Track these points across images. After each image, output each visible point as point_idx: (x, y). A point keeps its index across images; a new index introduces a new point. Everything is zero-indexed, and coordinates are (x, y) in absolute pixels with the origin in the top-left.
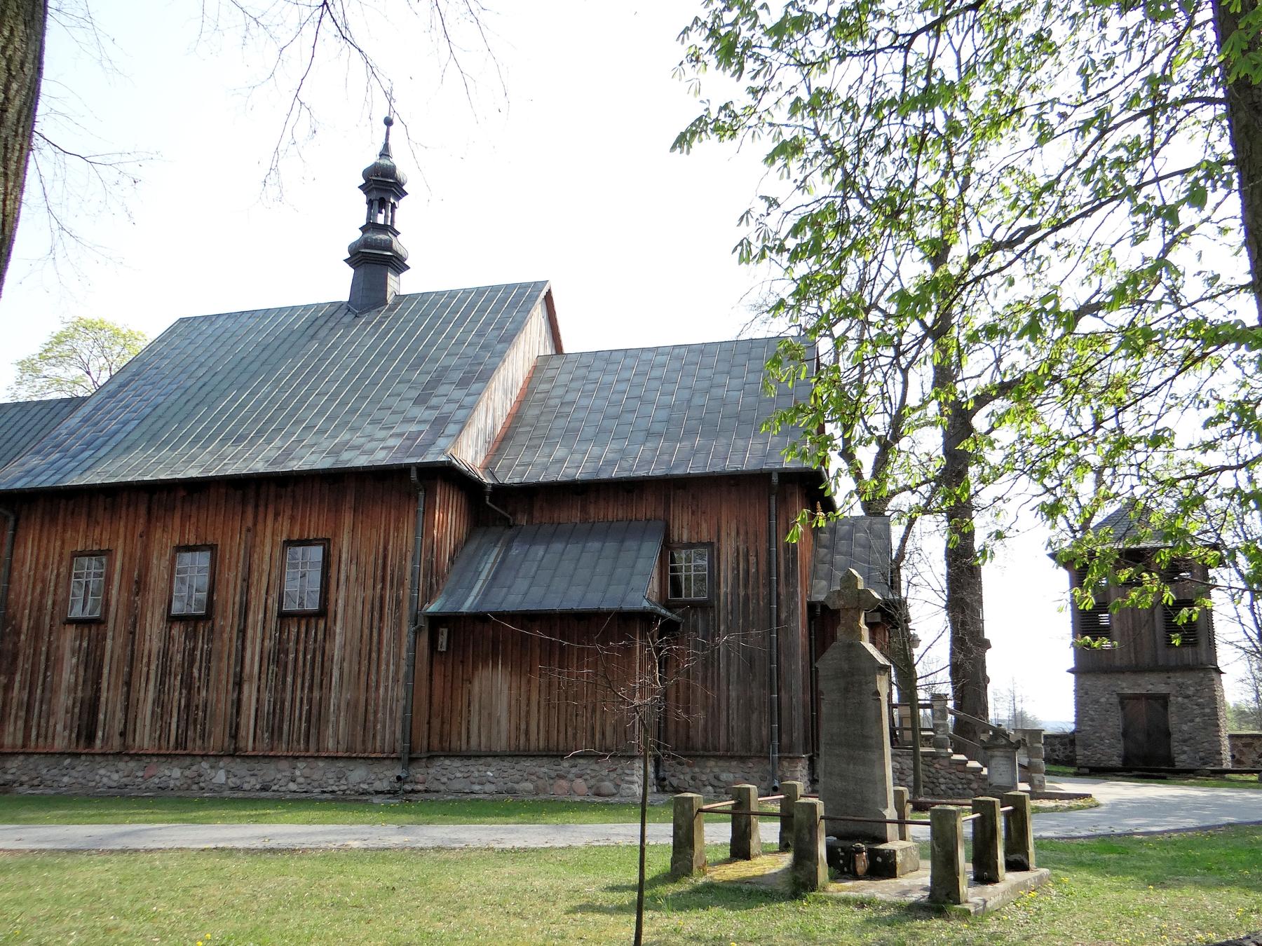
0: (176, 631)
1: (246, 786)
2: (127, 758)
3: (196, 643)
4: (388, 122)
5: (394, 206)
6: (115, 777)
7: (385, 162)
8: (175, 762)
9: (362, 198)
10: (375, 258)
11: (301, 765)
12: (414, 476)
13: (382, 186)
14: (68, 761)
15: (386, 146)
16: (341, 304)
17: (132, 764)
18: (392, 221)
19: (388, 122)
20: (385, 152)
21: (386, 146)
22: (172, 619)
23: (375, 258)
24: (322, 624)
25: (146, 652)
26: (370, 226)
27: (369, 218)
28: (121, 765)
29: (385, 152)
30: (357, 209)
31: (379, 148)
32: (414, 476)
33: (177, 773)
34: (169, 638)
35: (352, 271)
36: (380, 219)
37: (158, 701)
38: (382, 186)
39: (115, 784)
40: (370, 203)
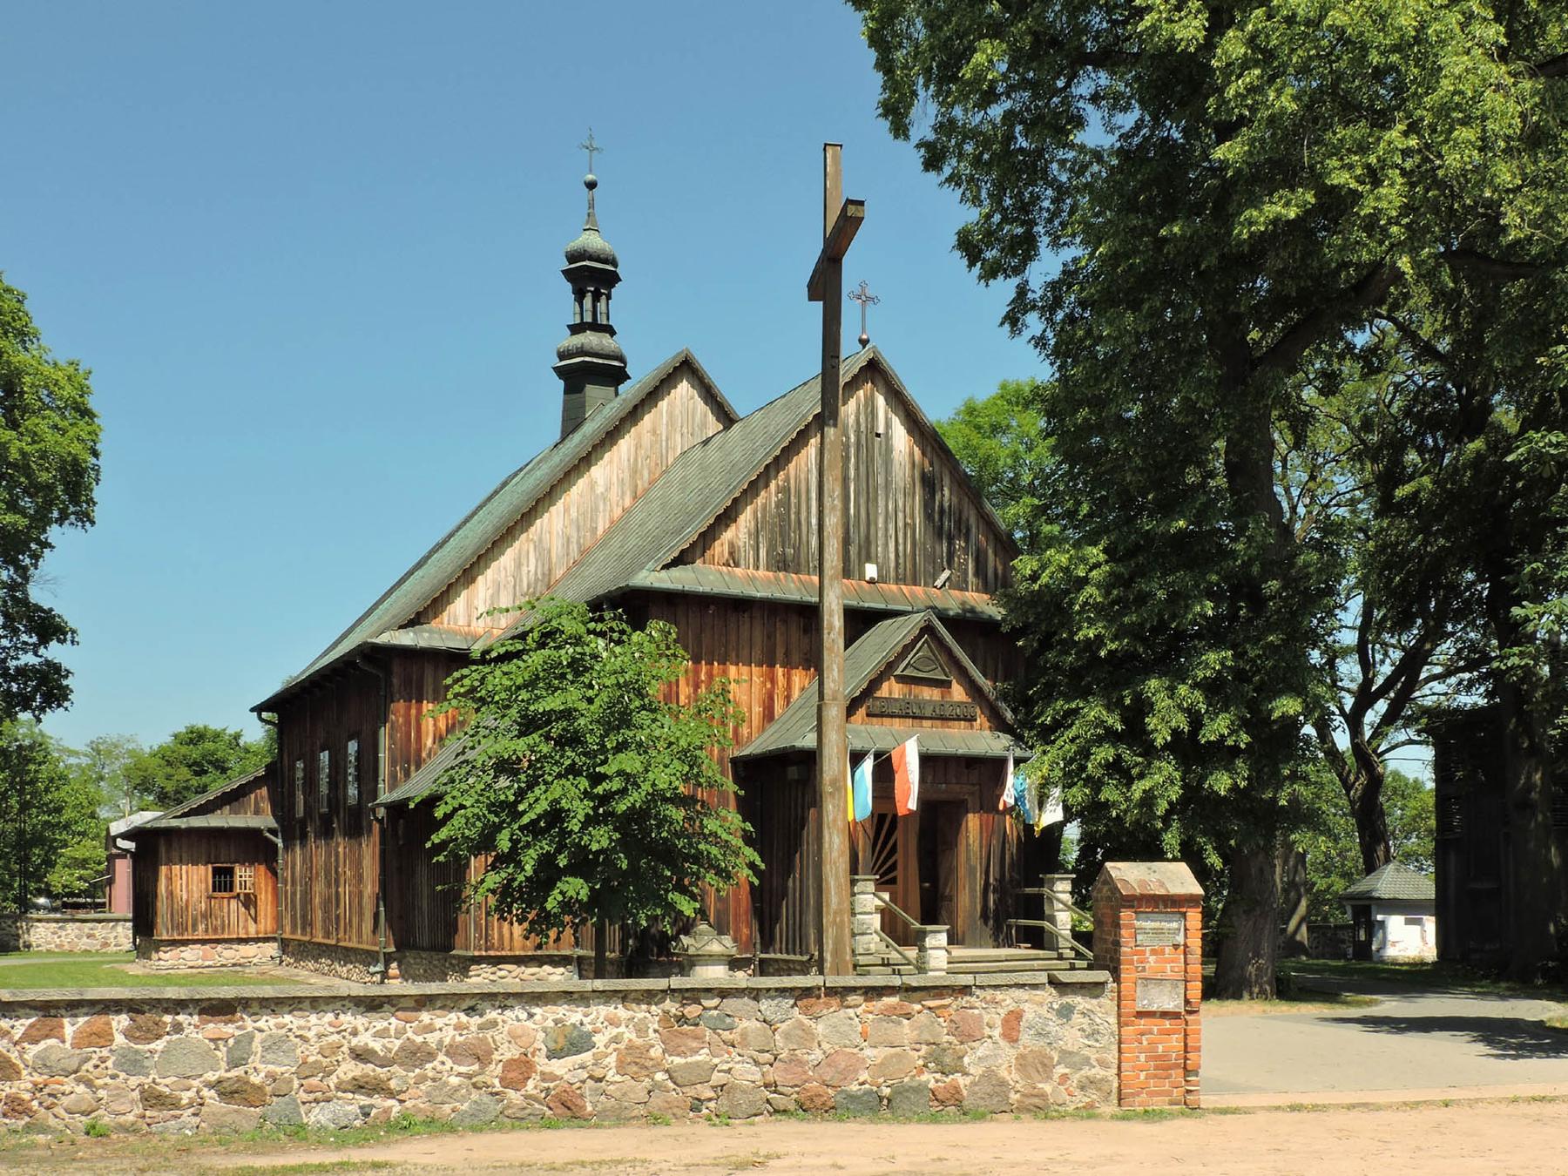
38: (592, 277)
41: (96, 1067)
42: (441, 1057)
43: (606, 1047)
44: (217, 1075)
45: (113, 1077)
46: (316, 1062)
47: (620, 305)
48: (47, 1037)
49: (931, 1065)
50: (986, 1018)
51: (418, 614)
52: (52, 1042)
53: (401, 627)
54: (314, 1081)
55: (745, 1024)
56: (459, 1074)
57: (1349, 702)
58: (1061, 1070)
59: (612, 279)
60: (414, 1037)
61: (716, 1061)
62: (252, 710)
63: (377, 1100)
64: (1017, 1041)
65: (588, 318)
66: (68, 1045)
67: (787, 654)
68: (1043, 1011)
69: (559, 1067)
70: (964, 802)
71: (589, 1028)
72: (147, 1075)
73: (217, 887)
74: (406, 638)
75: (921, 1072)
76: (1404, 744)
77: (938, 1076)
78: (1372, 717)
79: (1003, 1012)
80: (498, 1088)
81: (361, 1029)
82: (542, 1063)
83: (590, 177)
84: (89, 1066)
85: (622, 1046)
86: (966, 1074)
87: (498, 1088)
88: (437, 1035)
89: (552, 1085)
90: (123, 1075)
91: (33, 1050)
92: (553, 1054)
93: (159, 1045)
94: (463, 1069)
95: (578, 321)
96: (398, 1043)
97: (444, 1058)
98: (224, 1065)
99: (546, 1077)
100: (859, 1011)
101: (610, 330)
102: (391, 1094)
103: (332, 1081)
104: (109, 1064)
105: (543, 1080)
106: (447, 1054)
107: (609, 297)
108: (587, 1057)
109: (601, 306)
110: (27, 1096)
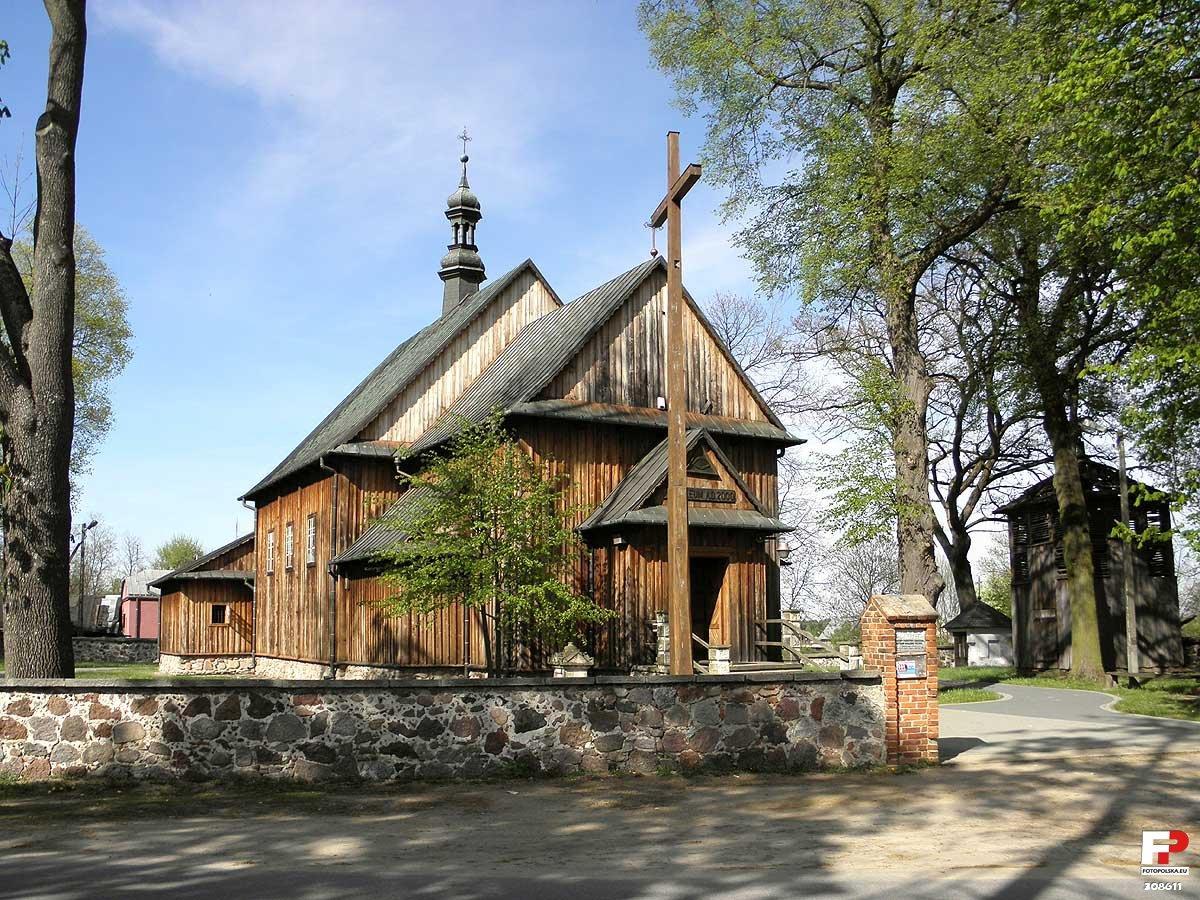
13: (467, 213)
38: (467, 213)
41: (230, 733)
42: (447, 731)
43: (554, 724)
44: (305, 741)
45: (241, 740)
46: (366, 733)
47: (481, 234)
48: (199, 713)
49: (765, 737)
50: (801, 704)
51: (360, 433)
52: (203, 715)
53: (349, 442)
54: (366, 745)
55: (644, 708)
56: (458, 743)
57: (945, 491)
58: (848, 740)
59: (477, 217)
60: (429, 717)
61: (625, 734)
62: (239, 499)
63: (405, 760)
64: (820, 720)
65: (460, 241)
66: (212, 718)
67: (369, 486)
68: (837, 698)
69: (525, 738)
70: (728, 558)
71: (542, 711)
72: (261, 740)
73: (215, 620)
74: (353, 449)
75: (758, 743)
76: (979, 521)
77: (770, 744)
78: (962, 501)
79: (811, 699)
80: (484, 753)
81: (396, 709)
82: (512, 735)
83: (463, 156)
84: (225, 732)
85: (564, 724)
86: (787, 742)
87: (484, 753)
88: (444, 715)
89: (519, 751)
90: (246, 740)
91: (191, 721)
92: (520, 729)
93: (269, 719)
94: (460, 739)
95: (454, 243)
96: (420, 720)
97: (449, 731)
98: (309, 733)
99: (516, 745)
100: (718, 699)
101: (474, 248)
102: (415, 756)
103: (377, 745)
104: (238, 731)
105: (513, 748)
106: (451, 729)
107: (474, 228)
108: (541, 731)
109: (469, 233)
110: (187, 752)
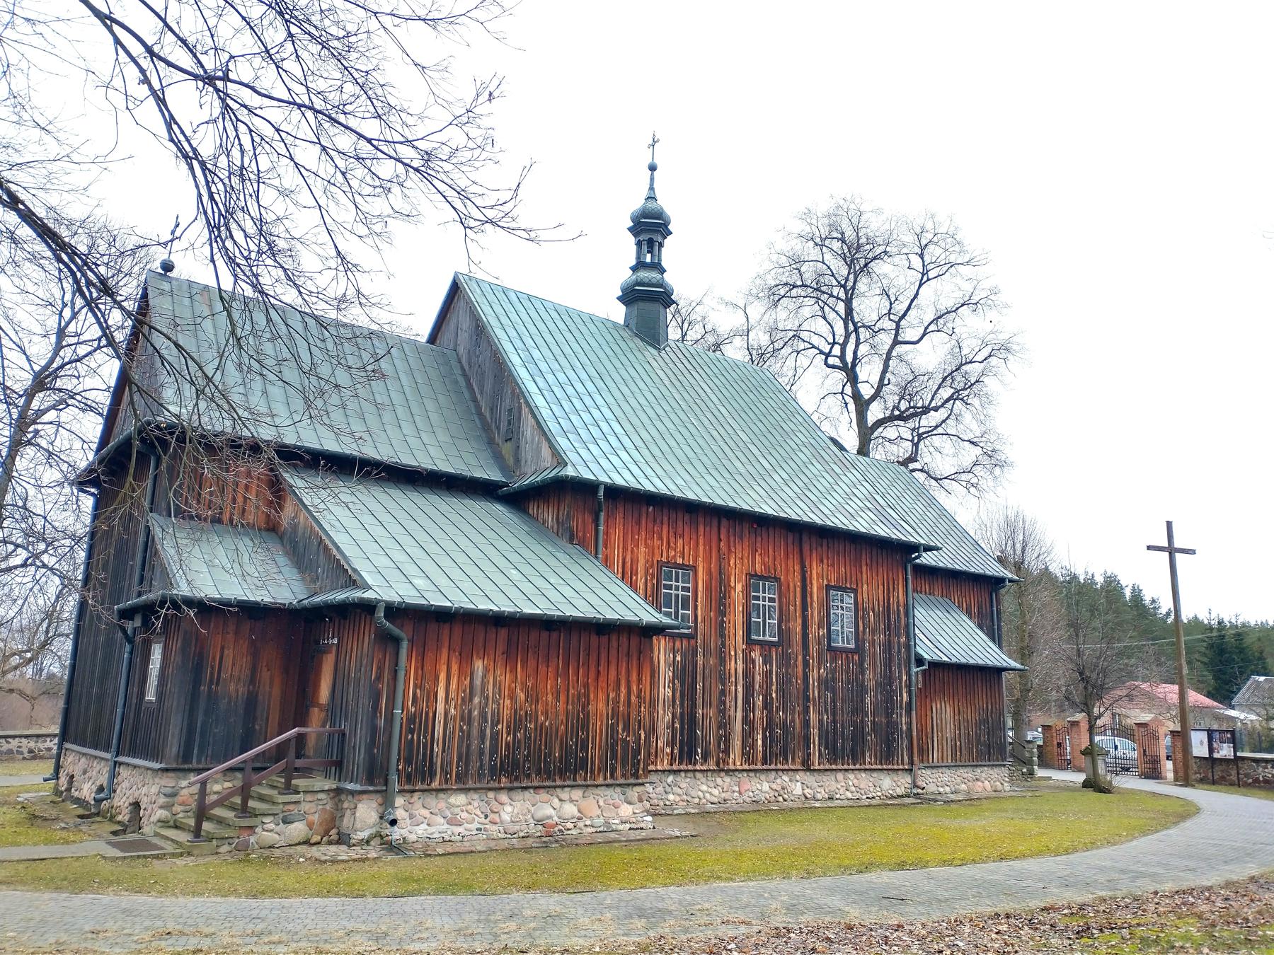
0: (756, 655)
1: (819, 796)
2: (723, 774)
3: (771, 666)
4: (653, 168)
5: (661, 245)
6: (716, 792)
7: (651, 205)
8: (763, 777)
9: (631, 240)
10: (647, 300)
11: (851, 776)
12: (601, 493)
13: (650, 228)
14: (670, 779)
15: (652, 188)
16: (615, 324)
17: (727, 779)
18: (659, 260)
19: (653, 168)
20: (651, 198)
21: (652, 188)
22: (750, 643)
23: (647, 300)
24: (856, 657)
25: (733, 672)
26: (639, 266)
27: (638, 257)
28: (719, 780)
29: (651, 198)
30: (628, 249)
31: (644, 192)
32: (601, 493)
33: (766, 787)
34: (749, 661)
35: (624, 308)
36: (648, 258)
37: (746, 720)
38: (650, 228)
39: (716, 800)
40: (639, 244)
